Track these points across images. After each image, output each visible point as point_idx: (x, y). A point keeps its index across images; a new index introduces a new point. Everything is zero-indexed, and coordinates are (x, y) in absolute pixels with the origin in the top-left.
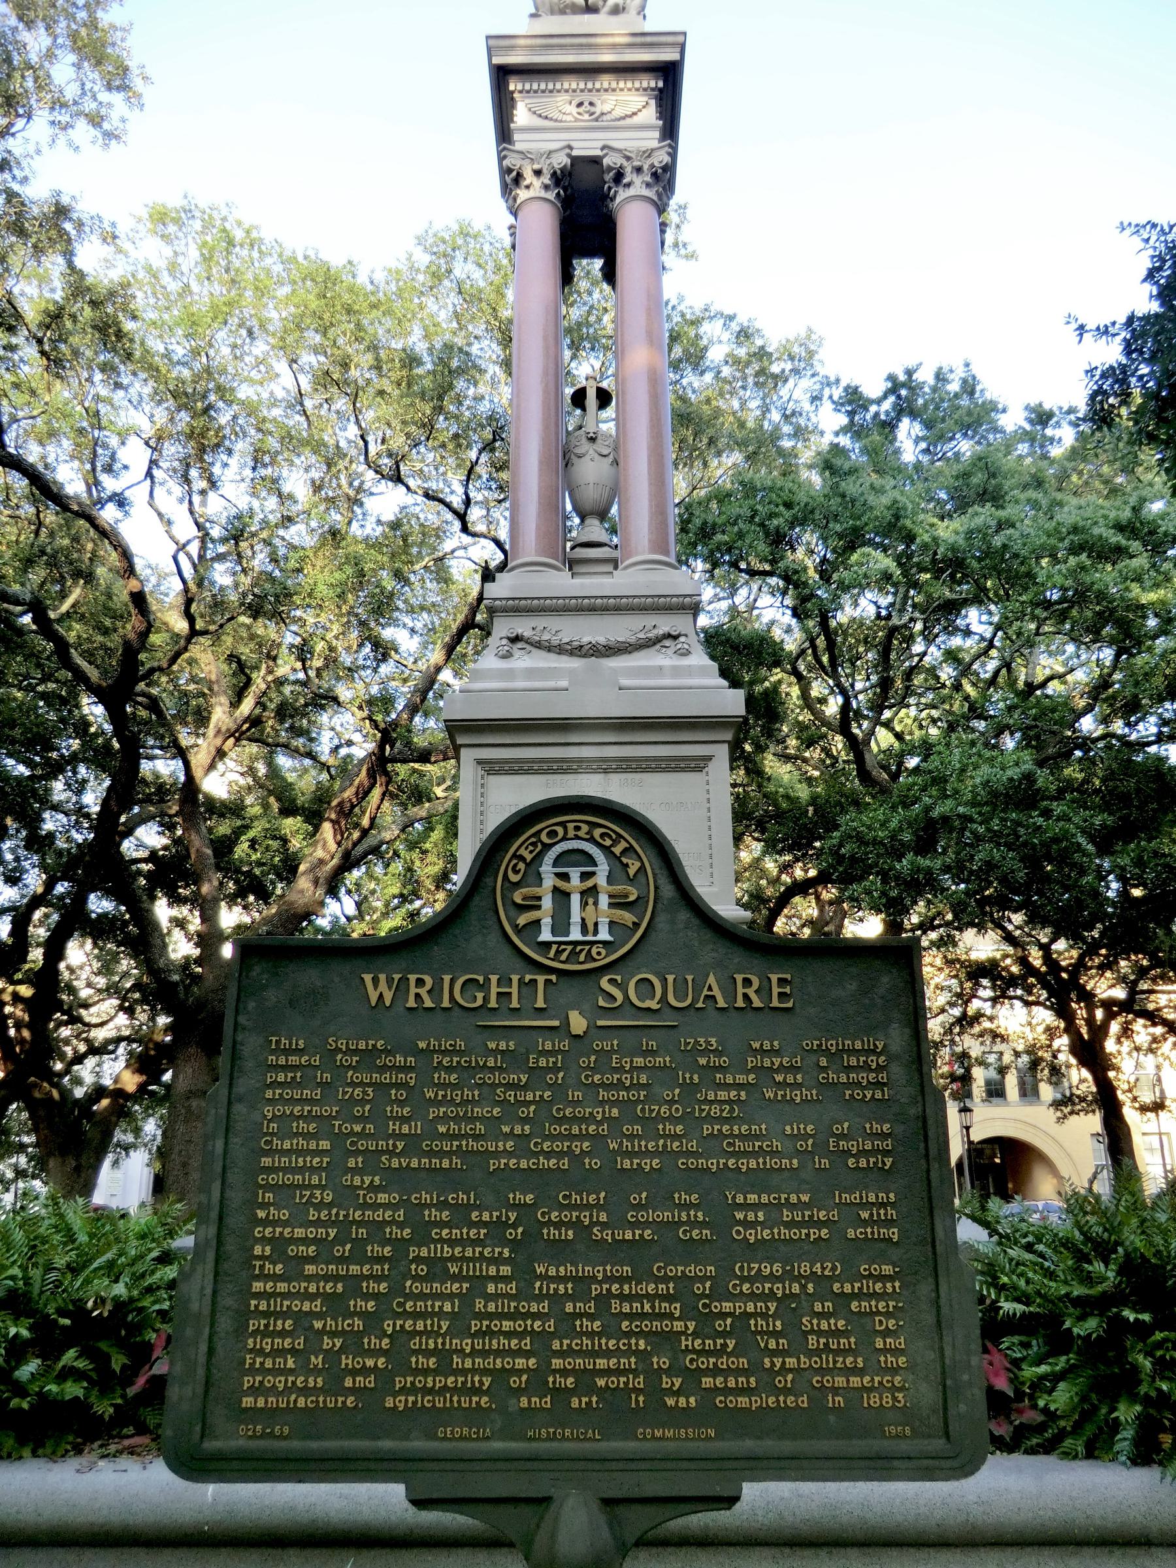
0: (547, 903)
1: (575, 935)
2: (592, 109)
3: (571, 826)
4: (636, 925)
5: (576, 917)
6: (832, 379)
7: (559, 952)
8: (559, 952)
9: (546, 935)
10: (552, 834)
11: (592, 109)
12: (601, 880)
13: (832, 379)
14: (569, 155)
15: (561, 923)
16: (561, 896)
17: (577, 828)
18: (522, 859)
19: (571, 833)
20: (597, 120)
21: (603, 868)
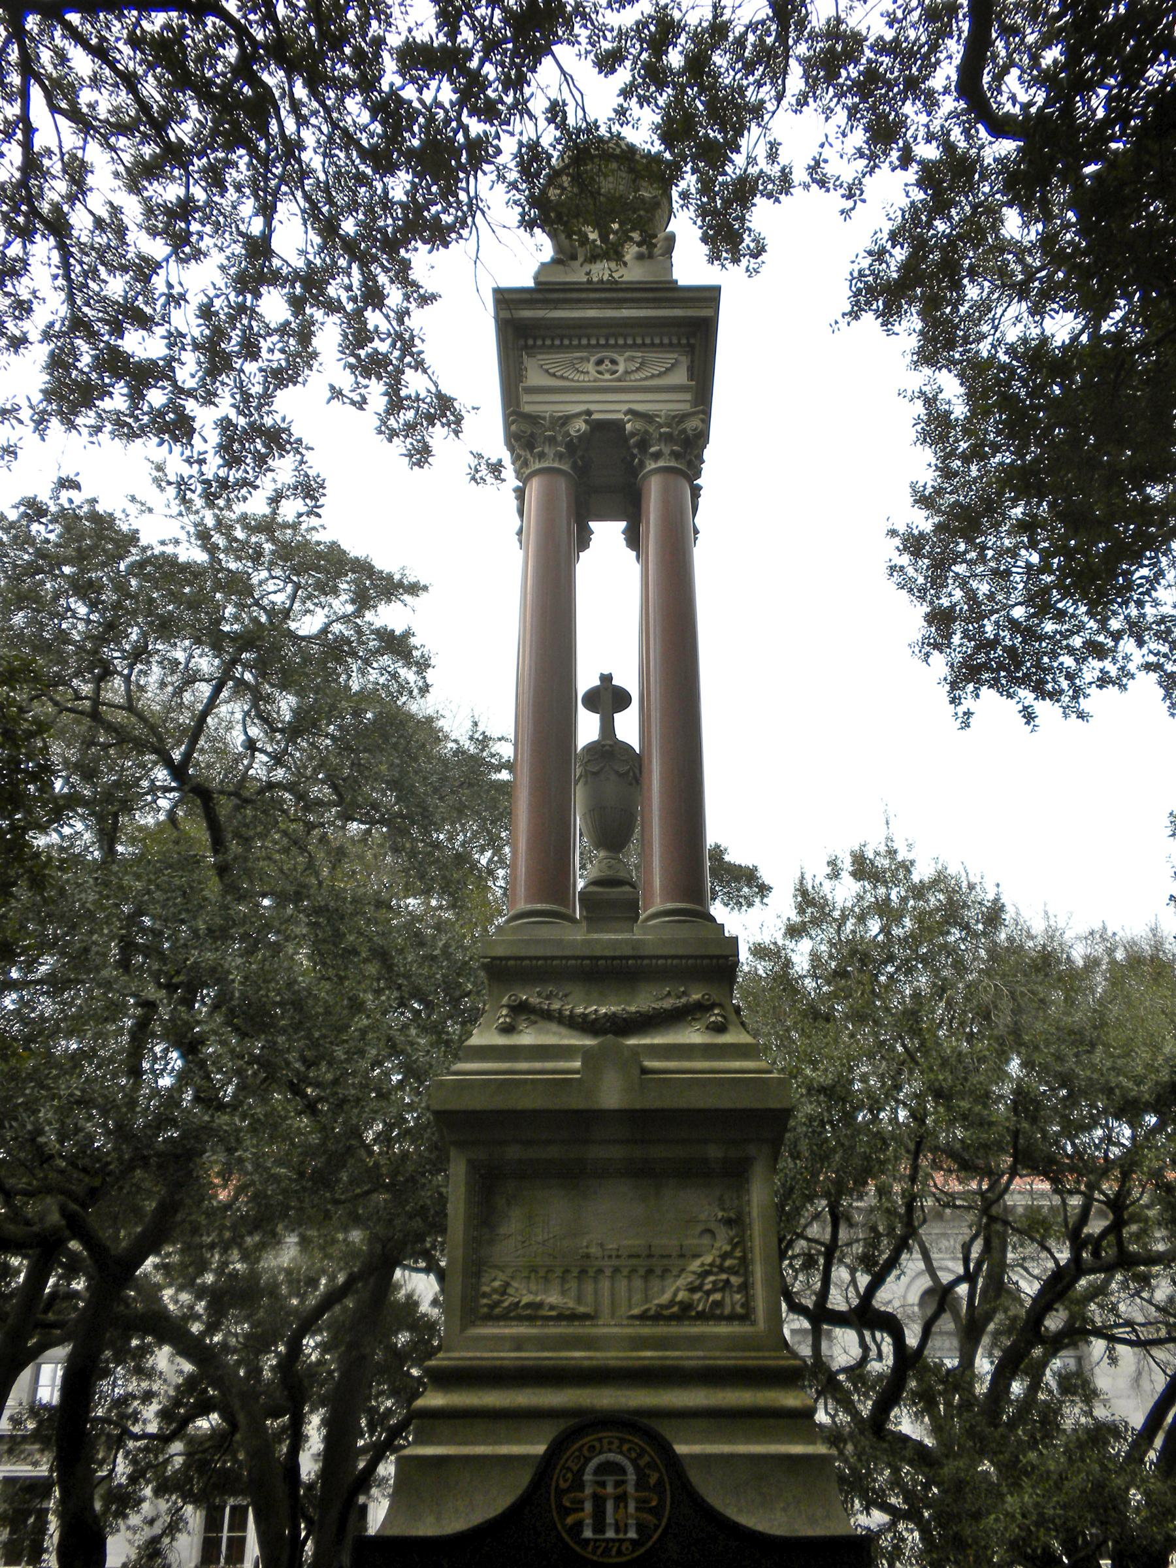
0: (588, 1506)
1: (610, 1534)
2: (615, 368)
3: (605, 1441)
4: (657, 1527)
5: (610, 1519)
6: (812, 163)
7: (596, 1548)
8: (596, 1548)
9: (588, 1534)
10: (592, 1448)
11: (615, 368)
12: (631, 1489)
13: (812, 163)
14: (586, 421)
15: (599, 1527)
16: (599, 1502)
17: (610, 1443)
18: (569, 1469)
19: (606, 1447)
20: (619, 380)
21: (631, 1477)
